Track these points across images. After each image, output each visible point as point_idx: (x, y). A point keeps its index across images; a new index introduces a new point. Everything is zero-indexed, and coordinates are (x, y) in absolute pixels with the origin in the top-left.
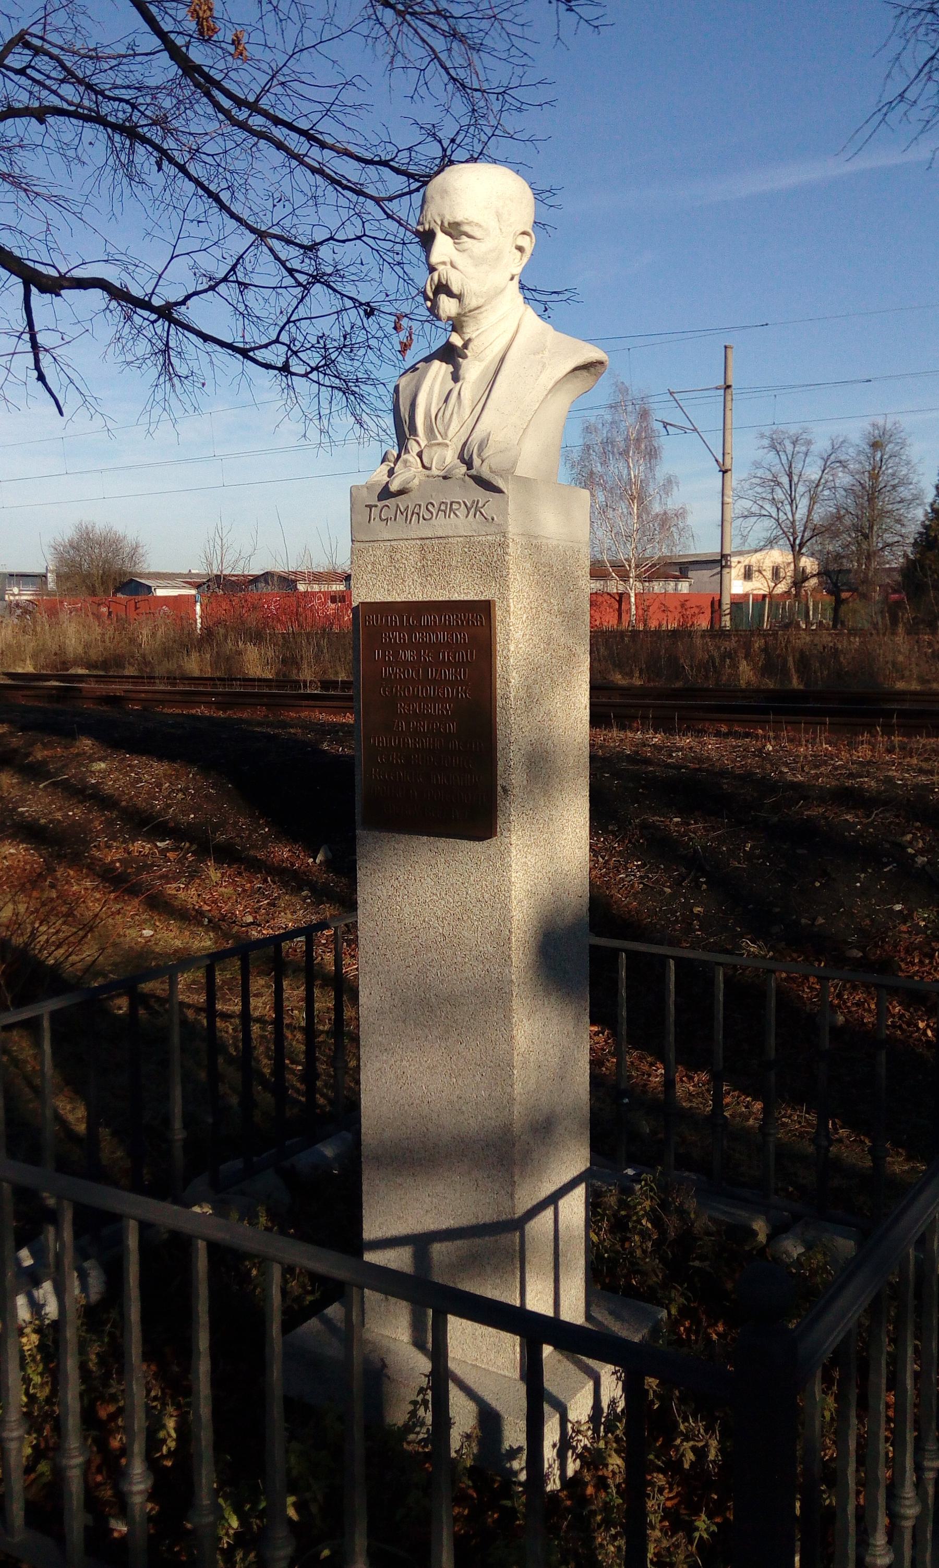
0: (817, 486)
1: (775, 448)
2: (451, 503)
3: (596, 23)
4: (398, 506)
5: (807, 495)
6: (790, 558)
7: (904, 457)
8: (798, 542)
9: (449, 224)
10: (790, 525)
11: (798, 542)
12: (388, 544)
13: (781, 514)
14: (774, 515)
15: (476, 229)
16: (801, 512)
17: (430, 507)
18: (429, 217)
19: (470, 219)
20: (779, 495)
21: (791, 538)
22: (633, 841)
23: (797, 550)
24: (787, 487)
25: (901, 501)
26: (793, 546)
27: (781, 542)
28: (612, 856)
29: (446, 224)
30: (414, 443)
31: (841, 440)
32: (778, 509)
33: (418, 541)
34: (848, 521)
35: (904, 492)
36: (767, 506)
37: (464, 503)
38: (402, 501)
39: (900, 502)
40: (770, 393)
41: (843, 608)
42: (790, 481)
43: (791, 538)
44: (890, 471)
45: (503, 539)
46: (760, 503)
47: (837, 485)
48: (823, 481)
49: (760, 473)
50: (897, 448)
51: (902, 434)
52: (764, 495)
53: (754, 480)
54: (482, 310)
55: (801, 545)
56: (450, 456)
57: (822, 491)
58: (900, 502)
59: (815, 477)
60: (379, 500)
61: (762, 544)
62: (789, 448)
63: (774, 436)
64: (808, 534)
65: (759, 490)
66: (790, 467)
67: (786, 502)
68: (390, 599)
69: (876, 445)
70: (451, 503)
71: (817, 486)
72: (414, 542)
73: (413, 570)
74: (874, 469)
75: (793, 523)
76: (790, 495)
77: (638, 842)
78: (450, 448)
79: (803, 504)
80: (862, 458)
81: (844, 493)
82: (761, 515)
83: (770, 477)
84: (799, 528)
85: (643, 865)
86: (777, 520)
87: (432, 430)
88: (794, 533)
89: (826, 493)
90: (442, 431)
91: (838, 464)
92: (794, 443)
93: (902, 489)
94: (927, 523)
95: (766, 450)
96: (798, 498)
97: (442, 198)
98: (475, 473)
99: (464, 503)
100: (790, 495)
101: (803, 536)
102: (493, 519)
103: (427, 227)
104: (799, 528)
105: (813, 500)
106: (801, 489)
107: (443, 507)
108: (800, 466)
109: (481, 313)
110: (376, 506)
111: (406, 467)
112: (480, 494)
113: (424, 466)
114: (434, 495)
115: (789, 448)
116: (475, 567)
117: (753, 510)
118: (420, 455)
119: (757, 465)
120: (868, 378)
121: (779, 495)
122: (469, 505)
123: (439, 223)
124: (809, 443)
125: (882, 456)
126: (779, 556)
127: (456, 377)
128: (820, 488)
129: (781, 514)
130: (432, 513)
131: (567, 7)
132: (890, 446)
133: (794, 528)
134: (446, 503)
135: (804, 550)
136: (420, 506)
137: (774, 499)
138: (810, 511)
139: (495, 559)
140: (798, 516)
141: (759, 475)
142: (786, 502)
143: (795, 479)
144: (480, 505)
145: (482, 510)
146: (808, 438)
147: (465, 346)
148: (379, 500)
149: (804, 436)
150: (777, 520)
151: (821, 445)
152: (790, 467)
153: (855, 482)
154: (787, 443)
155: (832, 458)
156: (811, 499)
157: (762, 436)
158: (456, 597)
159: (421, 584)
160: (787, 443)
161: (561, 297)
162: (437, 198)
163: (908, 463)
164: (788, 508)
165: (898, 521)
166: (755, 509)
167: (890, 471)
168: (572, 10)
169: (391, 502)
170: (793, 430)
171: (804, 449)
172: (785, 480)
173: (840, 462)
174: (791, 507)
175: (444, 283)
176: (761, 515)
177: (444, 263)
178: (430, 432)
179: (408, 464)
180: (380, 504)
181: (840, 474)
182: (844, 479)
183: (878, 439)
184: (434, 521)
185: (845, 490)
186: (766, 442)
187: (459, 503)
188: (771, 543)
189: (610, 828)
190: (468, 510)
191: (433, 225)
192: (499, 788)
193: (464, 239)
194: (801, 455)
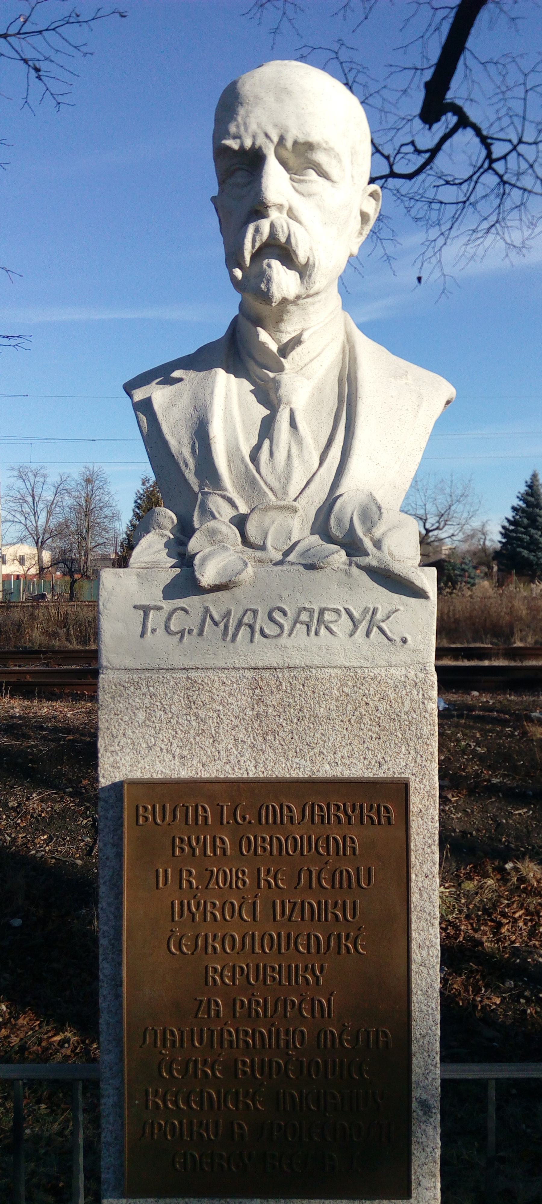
0: (52, 504)
1: (21, 477)
2: (322, 612)
3: (60, 99)
4: (207, 611)
5: (45, 509)
6: (35, 551)
7: (106, 490)
8: (40, 540)
9: (295, 143)
10: (34, 529)
11: (40, 540)
12: (183, 675)
13: (28, 522)
14: (23, 521)
15: (334, 162)
16: (42, 521)
17: (277, 615)
18: (253, 127)
19: (331, 144)
20: (26, 509)
21: (36, 538)
22: (35, 815)
23: (40, 545)
24: (31, 504)
25: (106, 517)
26: (37, 543)
27: (29, 540)
28: (18, 832)
29: (289, 144)
30: (220, 500)
31: (66, 476)
32: (26, 518)
33: (248, 674)
34: (73, 528)
35: (107, 512)
36: (18, 515)
37: (348, 611)
38: (216, 603)
39: (104, 518)
40: (27, 442)
41: (76, 585)
42: (33, 500)
43: (36, 538)
44: (97, 498)
45: (421, 675)
46: (13, 513)
47: (64, 504)
48: (55, 501)
49: (12, 493)
50: (101, 484)
51: (104, 475)
52: (16, 508)
53: (8, 498)
54: (317, 298)
55: (43, 543)
56: (299, 528)
57: (55, 507)
58: (104, 518)
59: (51, 498)
60: (165, 598)
61: (15, 540)
62: (32, 478)
63: (21, 470)
64: (46, 536)
65: (13, 504)
66: (33, 491)
67: (31, 514)
68: (185, 774)
69: (88, 481)
70: (322, 612)
71: (52, 504)
72: (238, 674)
73: (236, 722)
74: (87, 496)
75: (37, 527)
76: (34, 509)
77: (40, 815)
78: (298, 514)
79: (43, 516)
80: (80, 488)
81: (68, 509)
82: (14, 522)
83: (19, 496)
84: (40, 531)
85: (50, 839)
86: (26, 525)
87: (253, 482)
88: (37, 534)
89: (58, 509)
90: (276, 485)
91: (65, 491)
92: (35, 476)
93: (106, 509)
94: (129, 533)
95: (15, 479)
96: (39, 512)
97: (279, 100)
98: (375, 563)
99: (348, 611)
100: (34, 509)
101: (43, 537)
102: (404, 641)
103: (248, 143)
104: (40, 531)
105: (49, 513)
106: (41, 506)
107: (304, 617)
108: (40, 491)
109: (313, 304)
110: (159, 608)
111: (213, 542)
112: (382, 598)
113: (245, 541)
114: (285, 595)
115: (32, 478)
116: (366, 720)
117: (8, 517)
118: (240, 522)
119: (10, 488)
120: (94, 439)
121: (26, 509)
122: (356, 615)
123: (276, 139)
124: (45, 476)
125: (92, 488)
126: (27, 549)
127: (268, 395)
128: (54, 506)
129: (28, 522)
130: (281, 627)
131: (37, 75)
132: (97, 482)
133: (37, 532)
134: (311, 612)
135: (44, 546)
136: (255, 612)
137: (22, 511)
138: (47, 521)
139: (407, 708)
140: (39, 523)
141: (11, 494)
142: (31, 514)
143: (37, 499)
144: (379, 616)
145: (384, 625)
146: (45, 472)
147: (285, 350)
148: (165, 598)
149: (41, 471)
150: (26, 525)
151: (53, 479)
152: (33, 491)
153: (75, 503)
154: (30, 474)
155: (61, 487)
156: (48, 512)
157: (13, 469)
158: (326, 770)
159: (253, 746)
160: (30, 474)
161: (13, 342)
162: (269, 100)
163: (109, 494)
164: (32, 517)
165: (104, 530)
166: (9, 517)
167: (97, 498)
168: (40, 79)
169: (193, 602)
170: (34, 466)
171: (42, 480)
172: (29, 499)
173: (66, 490)
174: (35, 517)
175: (283, 240)
176: (14, 522)
177: (280, 207)
178: (249, 484)
179: (218, 537)
180: (168, 605)
181: (67, 498)
182: (68, 501)
183: (89, 477)
184: (284, 640)
185: (70, 508)
186: (16, 473)
187: (337, 611)
188: (21, 540)
189: (10, 804)
190: (355, 627)
191: (261, 141)
192: (415, 1105)
193: (312, 175)
194: (40, 483)
